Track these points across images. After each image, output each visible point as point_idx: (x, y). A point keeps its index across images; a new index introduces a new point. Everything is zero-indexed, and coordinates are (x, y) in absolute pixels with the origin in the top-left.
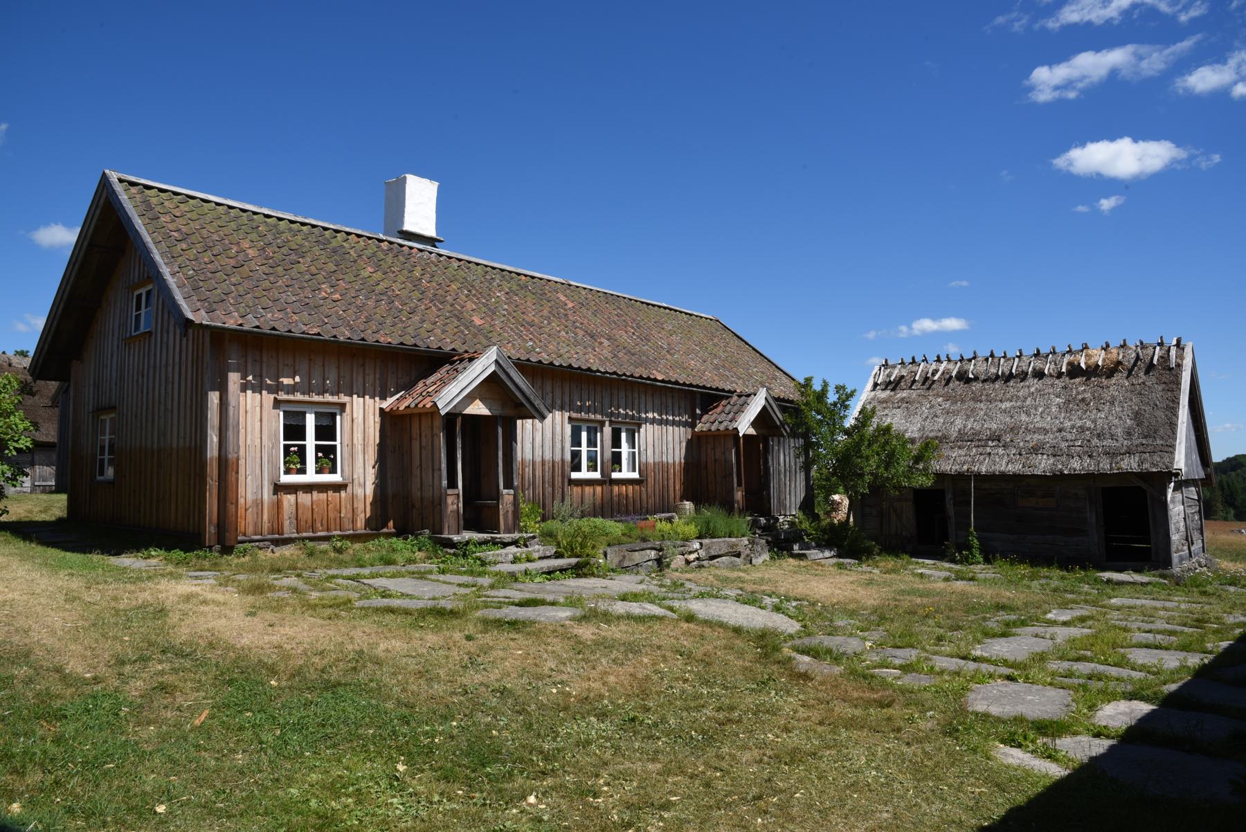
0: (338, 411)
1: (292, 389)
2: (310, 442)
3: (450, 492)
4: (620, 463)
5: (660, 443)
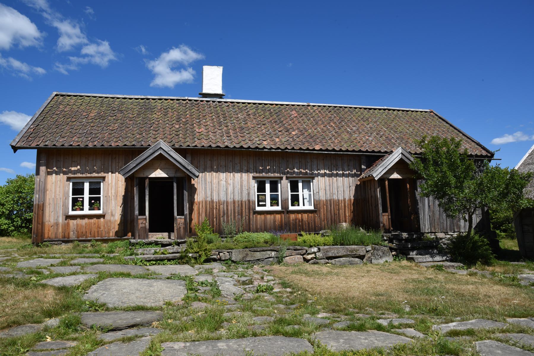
0: (102, 181)
1: (75, 172)
2: (86, 196)
3: (140, 217)
4: (298, 200)
5: (335, 188)
